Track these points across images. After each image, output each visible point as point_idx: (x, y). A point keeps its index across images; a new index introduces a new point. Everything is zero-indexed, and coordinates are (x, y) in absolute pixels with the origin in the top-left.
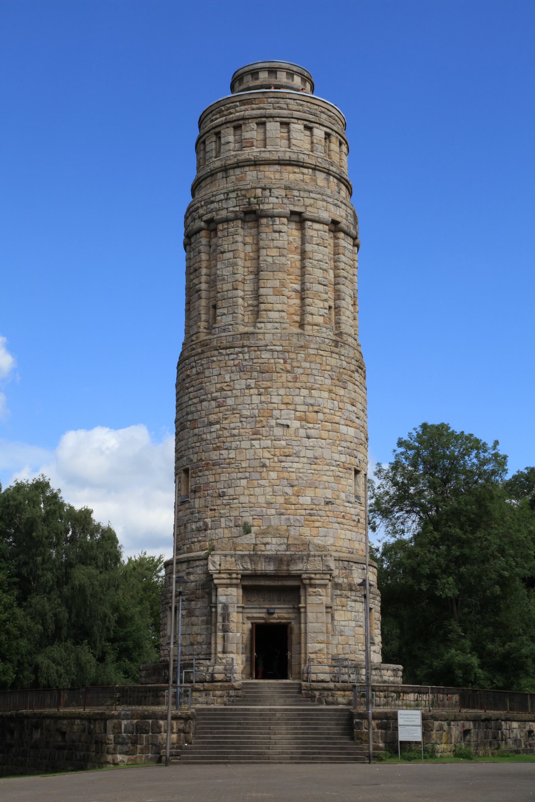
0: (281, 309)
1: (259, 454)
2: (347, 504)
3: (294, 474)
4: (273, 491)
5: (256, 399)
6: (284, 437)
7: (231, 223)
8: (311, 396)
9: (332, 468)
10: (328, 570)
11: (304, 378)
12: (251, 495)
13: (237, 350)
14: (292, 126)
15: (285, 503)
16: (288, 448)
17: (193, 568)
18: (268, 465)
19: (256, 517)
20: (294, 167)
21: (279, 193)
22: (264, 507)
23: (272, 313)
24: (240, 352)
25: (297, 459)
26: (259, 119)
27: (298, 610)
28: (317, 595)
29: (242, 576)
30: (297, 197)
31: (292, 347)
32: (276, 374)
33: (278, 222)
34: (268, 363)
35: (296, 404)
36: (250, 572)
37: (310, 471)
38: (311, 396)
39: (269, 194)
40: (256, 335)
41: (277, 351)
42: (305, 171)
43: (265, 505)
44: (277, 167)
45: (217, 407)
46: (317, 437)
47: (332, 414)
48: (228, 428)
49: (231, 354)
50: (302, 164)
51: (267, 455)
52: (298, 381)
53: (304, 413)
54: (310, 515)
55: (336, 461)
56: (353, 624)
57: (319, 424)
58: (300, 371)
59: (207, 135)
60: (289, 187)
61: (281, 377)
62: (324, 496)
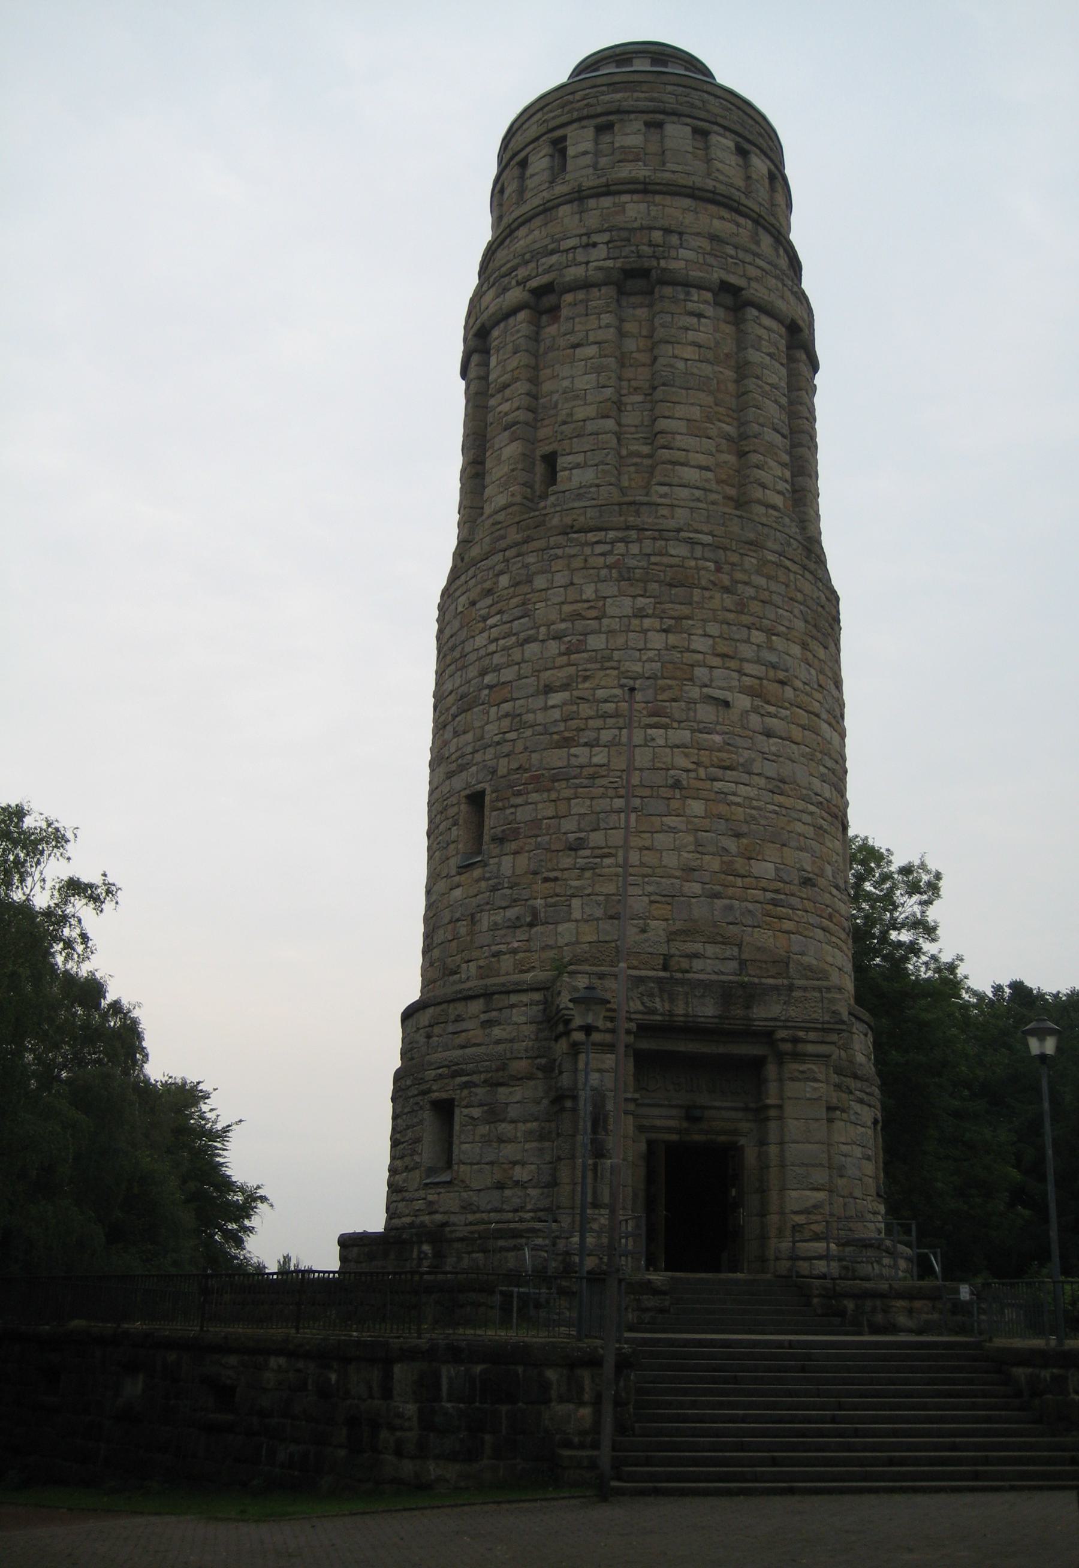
0: (704, 463)
1: (665, 759)
2: (834, 891)
3: (740, 809)
4: (698, 844)
5: (657, 640)
6: (718, 727)
7: (596, 289)
8: (771, 649)
9: (812, 808)
10: (836, 1023)
11: (755, 607)
12: (647, 849)
13: (612, 534)
14: (714, 139)
15: (724, 873)
16: (728, 751)
17: (500, 1009)
18: (685, 783)
19: (658, 898)
20: (721, 209)
21: (700, 244)
22: (677, 878)
23: (686, 469)
24: (622, 540)
25: (746, 776)
26: (651, 116)
27: (760, 1114)
28: (808, 1079)
29: (640, 1027)
30: (732, 257)
31: (732, 540)
32: (699, 591)
33: (695, 298)
34: (682, 566)
35: (742, 660)
36: (659, 1018)
37: (771, 807)
38: (771, 649)
39: (678, 242)
40: (654, 507)
41: (702, 544)
42: (742, 220)
43: (678, 873)
44: (688, 202)
45: (564, 654)
46: (784, 735)
47: (807, 694)
48: (591, 698)
49: (597, 543)
50: (736, 205)
51: (682, 762)
52: (746, 610)
53: (757, 681)
54: (775, 903)
55: (816, 794)
56: (858, 1152)
57: (786, 709)
58: (750, 591)
59: (531, 147)
60: (718, 236)
61: (711, 597)
62: (798, 866)
